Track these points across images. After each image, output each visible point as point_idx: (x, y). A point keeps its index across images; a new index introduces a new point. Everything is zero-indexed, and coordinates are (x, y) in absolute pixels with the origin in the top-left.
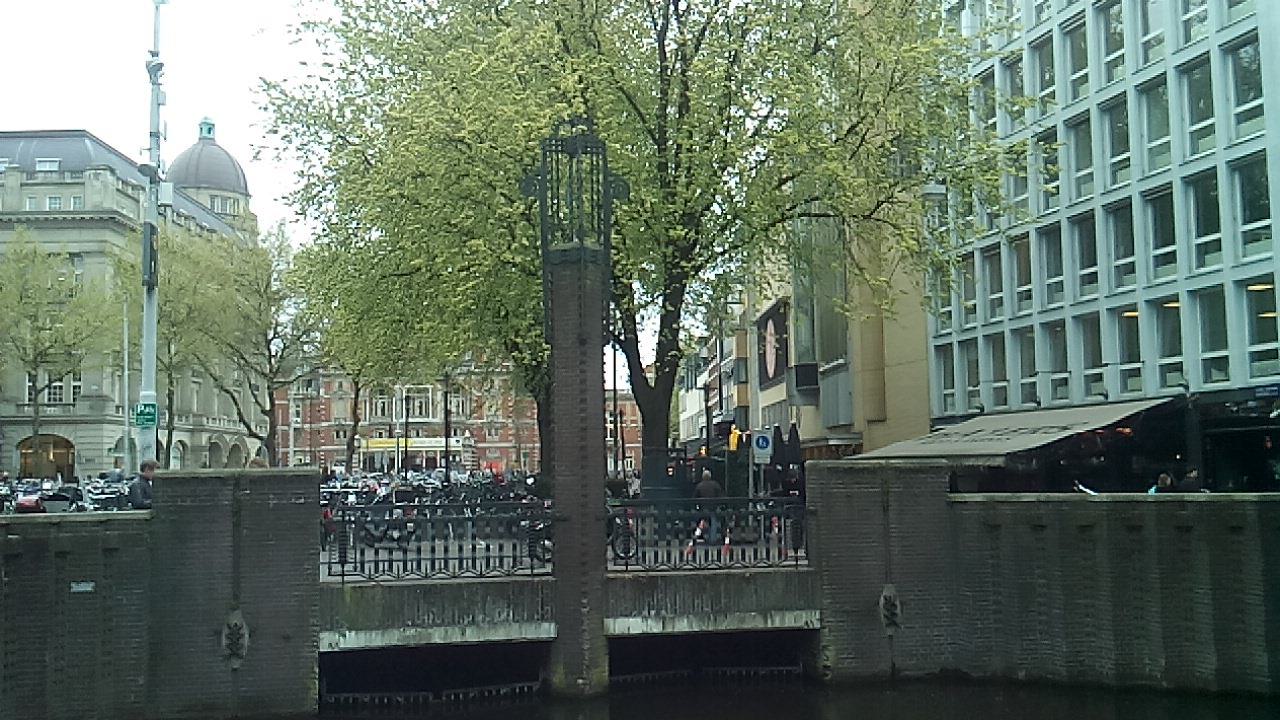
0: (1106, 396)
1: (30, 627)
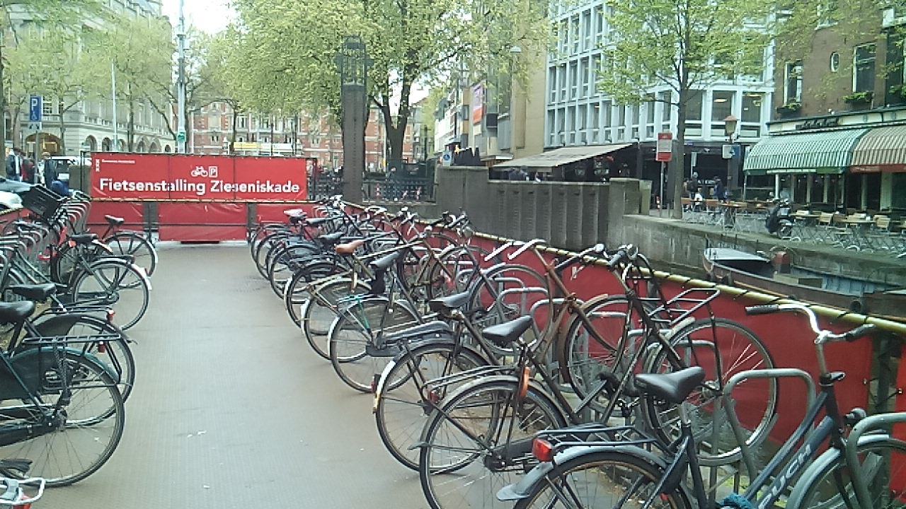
0: (611, 141)
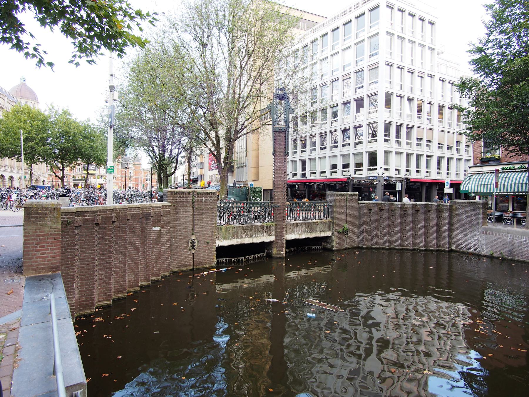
1: (32, 239)
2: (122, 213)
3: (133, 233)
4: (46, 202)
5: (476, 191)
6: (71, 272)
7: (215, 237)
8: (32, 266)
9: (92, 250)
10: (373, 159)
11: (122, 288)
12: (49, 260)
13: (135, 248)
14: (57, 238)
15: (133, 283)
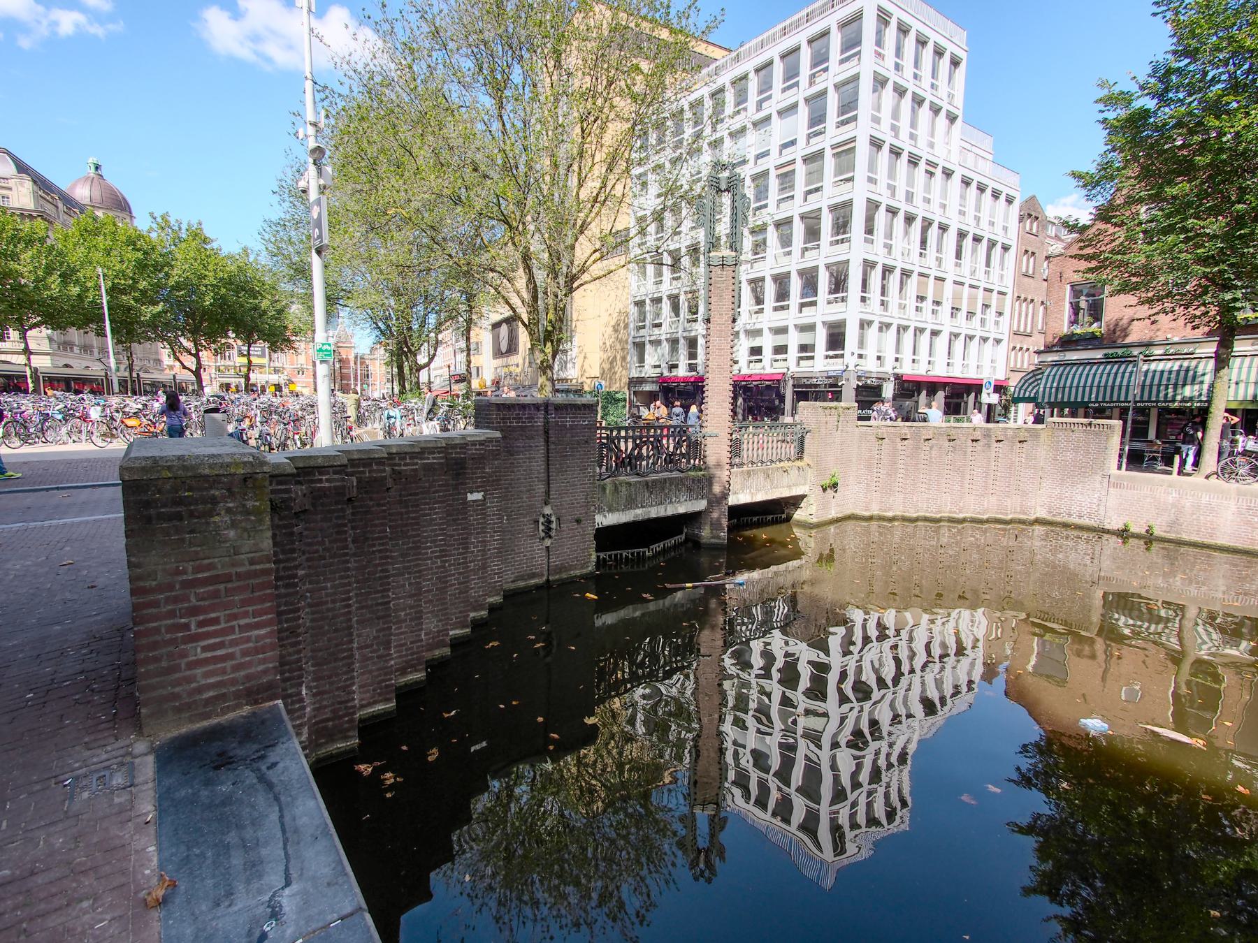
1: (167, 600)
2: (406, 465)
3: (430, 515)
4: (213, 456)
5: (1052, 400)
6: (290, 655)
7: (593, 508)
8: (176, 697)
9: (341, 577)
10: (836, 340)
11: (413, 659)
12: (237, 668)
13: (436, 552)
14: (263, 586)
15: (433, 638)
